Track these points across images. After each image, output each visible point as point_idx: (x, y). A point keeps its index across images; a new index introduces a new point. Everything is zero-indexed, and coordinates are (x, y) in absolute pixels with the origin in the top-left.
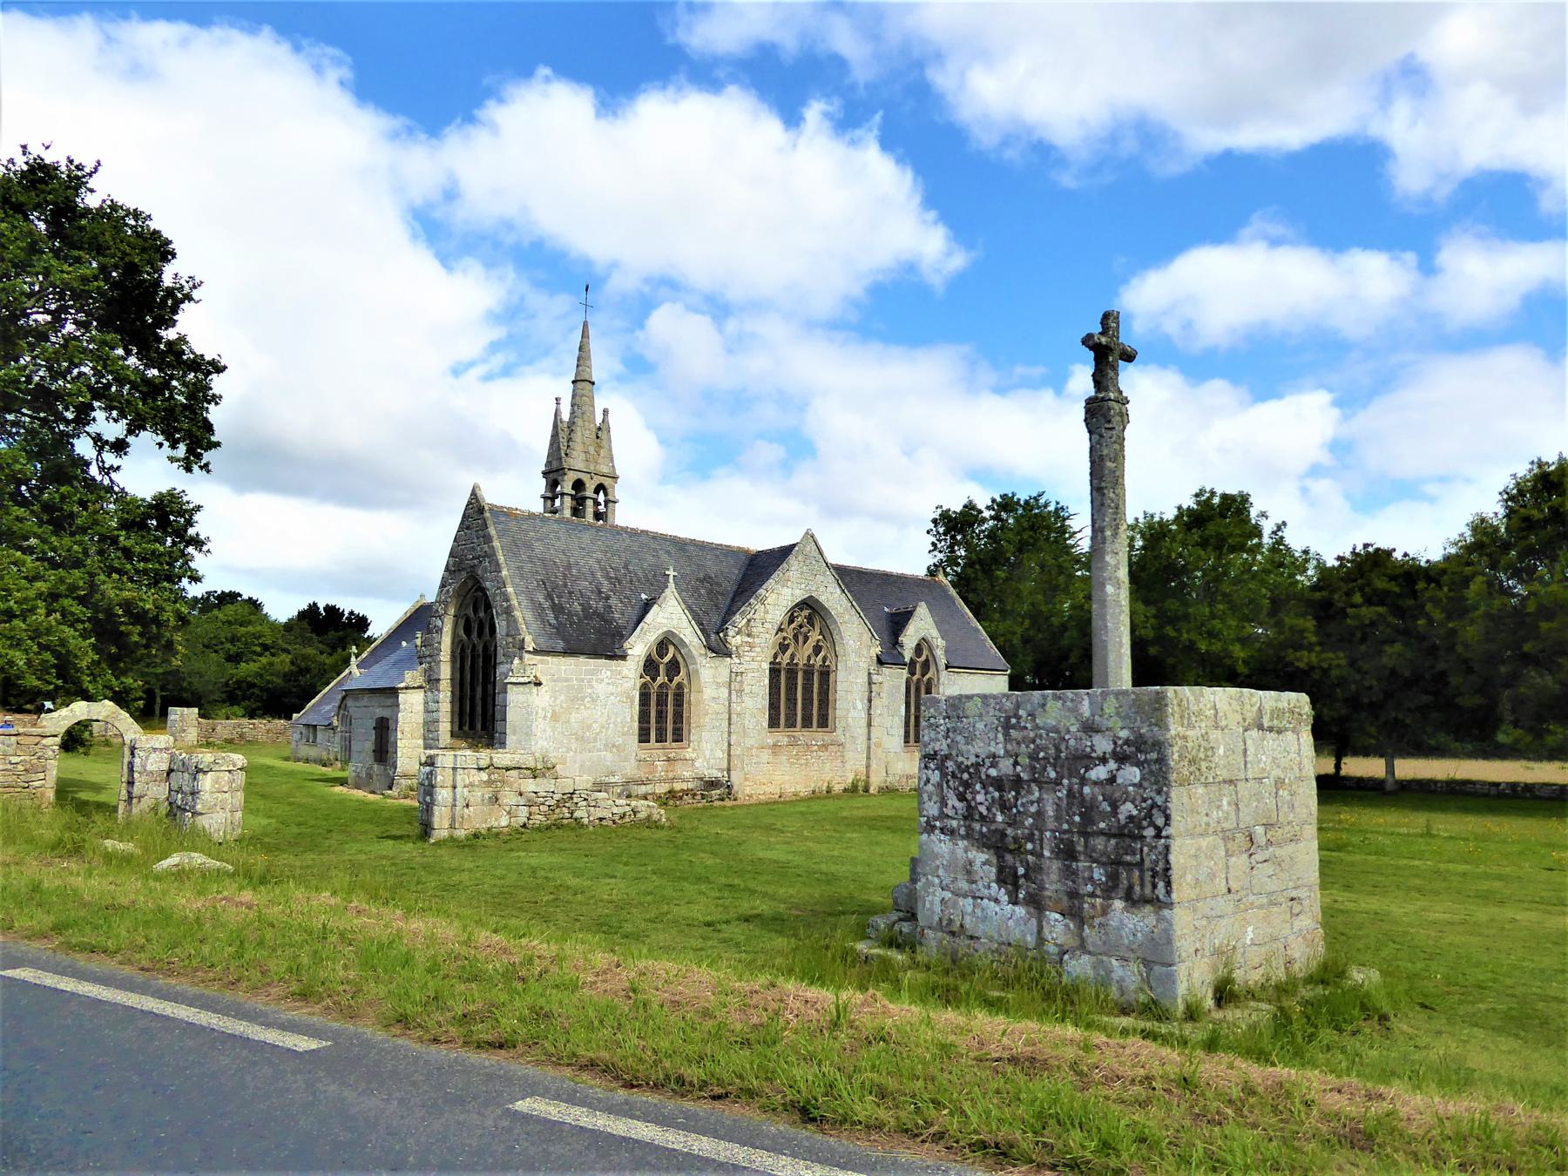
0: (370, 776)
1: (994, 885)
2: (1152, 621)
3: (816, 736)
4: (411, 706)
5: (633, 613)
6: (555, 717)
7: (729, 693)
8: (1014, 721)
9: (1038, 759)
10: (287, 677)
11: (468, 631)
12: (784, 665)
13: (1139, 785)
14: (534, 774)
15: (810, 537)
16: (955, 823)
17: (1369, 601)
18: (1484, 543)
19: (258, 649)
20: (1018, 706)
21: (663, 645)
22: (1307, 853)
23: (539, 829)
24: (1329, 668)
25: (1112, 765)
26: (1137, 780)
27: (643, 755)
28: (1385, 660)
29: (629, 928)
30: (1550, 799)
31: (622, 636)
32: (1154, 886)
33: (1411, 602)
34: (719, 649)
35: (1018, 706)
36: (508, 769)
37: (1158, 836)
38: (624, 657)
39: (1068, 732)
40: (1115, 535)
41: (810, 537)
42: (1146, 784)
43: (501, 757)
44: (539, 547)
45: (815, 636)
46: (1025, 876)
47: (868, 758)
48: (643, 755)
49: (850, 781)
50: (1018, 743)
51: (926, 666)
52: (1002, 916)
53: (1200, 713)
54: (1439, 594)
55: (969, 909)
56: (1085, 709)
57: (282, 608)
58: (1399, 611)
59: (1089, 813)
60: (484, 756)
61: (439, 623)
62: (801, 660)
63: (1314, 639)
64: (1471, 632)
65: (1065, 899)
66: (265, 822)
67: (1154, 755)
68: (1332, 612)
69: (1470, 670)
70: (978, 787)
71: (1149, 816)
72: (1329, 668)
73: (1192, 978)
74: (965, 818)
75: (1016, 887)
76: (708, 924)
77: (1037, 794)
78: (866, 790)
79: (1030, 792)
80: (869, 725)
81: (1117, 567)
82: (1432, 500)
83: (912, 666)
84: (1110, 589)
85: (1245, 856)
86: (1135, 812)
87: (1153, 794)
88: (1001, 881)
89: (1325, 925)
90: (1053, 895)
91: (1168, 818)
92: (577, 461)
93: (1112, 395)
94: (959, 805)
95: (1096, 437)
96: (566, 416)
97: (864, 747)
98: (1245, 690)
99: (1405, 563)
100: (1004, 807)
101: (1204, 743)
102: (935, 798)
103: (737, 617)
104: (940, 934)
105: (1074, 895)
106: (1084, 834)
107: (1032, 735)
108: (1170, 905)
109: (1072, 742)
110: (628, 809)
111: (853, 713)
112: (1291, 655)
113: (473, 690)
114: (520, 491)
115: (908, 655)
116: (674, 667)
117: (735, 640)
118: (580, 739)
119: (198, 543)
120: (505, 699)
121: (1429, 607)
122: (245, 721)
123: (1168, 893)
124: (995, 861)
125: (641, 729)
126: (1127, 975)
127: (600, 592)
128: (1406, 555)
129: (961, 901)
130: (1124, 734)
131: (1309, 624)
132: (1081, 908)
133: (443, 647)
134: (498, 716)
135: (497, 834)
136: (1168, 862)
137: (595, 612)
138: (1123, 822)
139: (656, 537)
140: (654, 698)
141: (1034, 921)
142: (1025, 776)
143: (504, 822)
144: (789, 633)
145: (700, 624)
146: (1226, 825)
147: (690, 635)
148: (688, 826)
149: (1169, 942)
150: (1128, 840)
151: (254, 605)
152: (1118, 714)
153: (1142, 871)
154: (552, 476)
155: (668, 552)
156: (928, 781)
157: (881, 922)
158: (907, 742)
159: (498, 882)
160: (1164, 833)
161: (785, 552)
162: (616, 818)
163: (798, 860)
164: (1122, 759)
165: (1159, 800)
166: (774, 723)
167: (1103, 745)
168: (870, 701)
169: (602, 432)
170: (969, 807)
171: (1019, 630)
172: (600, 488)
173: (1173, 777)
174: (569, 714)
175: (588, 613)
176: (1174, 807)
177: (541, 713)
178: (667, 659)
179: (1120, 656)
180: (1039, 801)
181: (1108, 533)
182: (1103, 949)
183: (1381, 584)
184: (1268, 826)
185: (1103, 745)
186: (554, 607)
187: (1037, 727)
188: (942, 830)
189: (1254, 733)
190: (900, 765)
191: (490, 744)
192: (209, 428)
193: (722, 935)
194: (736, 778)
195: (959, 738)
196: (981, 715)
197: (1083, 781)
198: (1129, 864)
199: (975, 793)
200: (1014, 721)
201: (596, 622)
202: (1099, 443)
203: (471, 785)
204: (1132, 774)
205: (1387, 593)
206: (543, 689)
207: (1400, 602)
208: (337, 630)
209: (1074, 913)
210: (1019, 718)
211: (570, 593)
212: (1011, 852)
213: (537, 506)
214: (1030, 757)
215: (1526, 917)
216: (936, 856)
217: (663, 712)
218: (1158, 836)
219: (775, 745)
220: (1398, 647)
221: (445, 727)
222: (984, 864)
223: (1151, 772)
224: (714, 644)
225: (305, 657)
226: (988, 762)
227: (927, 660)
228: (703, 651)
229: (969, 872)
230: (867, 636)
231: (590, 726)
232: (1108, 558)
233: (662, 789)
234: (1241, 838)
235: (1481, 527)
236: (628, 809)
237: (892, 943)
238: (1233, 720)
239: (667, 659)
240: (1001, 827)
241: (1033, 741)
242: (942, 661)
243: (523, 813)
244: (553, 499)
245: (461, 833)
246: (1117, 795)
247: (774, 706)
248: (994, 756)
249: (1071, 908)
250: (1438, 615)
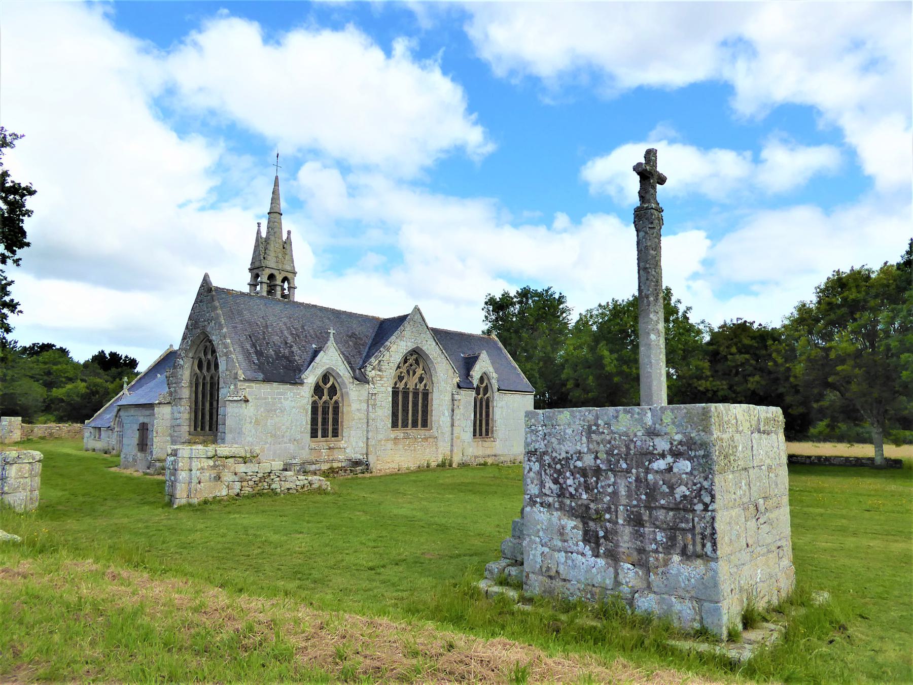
0: (135, 460)
1: (581, 543)
2: (615, 362)
3: (420, 432)
4: (163, 416)
5: (307, 357)
6: (257, 423)
7: (367, 407)
8: (594, 428)
9: (613, 455)
10: (83, 396)
11: (200, 366)
12: (401, 389)
13: (691, 473)
14: (245, 460)
15: (417, 310)
16: (551, 500)
17: (740, 352)
18: (805, 318)
19: (64, 380)
20: (597, 418)
21: (325, 377)
22: (783, 514)
23: (248, 497)
24: (717, 391)
25: (669, 459)
26: (689, 470)
27: (313, 445)
28: (749, 385)
29: (316, 574)
30: (840, 465)
31: (300, 371)
32: (704, 546)
33: (764, 352)
34: (361, 378)
35: (597, 418)
36: (226, 458)
37: (706, 509)
38: (302, 384)
39: (636, 436)
40: (656, 300)
41: (417, 310)
42: (696, 473)
43: (223, 450)
44: (247, 315)
45: (419, 371)
46: (605, 537)
47: (452, 446)
48: (313, 445)
49: (440, 460)
50: (598, 443)
51: (486, 390)
52: (585, 568)
53: (728, 422)
54: (781, 347)
55: (563, 560)
56: (649, 419)
57: (81, 354)
58: (757, 357)
59: (652, 492)
60: (211, 449)
61: (181, 362)
62: (411, 386)
63: (708, 373)
64: (799, 368)
65: (635, 553)
66: (60, 494)
67: (702, 453)
68: (718, 357)
69: (797, 392)
70: (568, 474)
71: (699, 495)
72: (717, 391)
73: (729, 612)
74: (559, 496)
75: (598, 545)
76: (371, 569)
77: (613, 480)
78: (450, 465)
79: (607, 478)
80: (452, 425)
81: (657, 322)
82: (756, 294)
83: (478, 390)
84: (653, 337)
85: (754, 520)
86: (688, 493)
87: (701, 480)
88: (586, 540)
89: (794, 563)
90: (626, 551)
91: (713, 497)
92: (271, 262)
93: (653, 206)
94: (554, 487)
95: (642, 234)
96: (264, 235)
97: (450, 439)
98: (751, 406)
99: (759, 330)
100: (588, 489)
101: (732, 443)
102: (535, 482)
103: (372, 359)
104: (540, 577)
105: (641, 551)
106: (648, 508)
107: (608, 438)
108: (716, 560)
109: (639, 443)
110: (306, 482)
111: (442, 418)
112: (695, 383)
113: (203, 405)
114: (235, 277)
115: (475, 383)
116: (333, 391)
117: (371, 374)
118: (274, 436)
119: (12, 306)
120: (225, 411)
121: (774, 355)
122: (53, 425)
123: (715, 551)
124: (581, 526)
125: (312, 429)
126: (684, 611)
127: (286, 343)
128: (760, 325)
129: (556, 554)
130: (678, 437)
131: (707, 364)
132: (647, 561)
133: (184, 378)
134: (220, 422)
135: (220, 501)
136: (713, 528)
137: (283, 356)
138: (678, 500)
139: (322, 309)
140: (320, 410)
141: (611, 570)
142: (603, 467)
143: (224, 493)
144: (404, 369)
145: (349, 363)
146: (745, 500)
147: (343, 370)
148: (345, 492)
149: (716, 585)
150: (682, 513)
151: (63, 352)
152: (673, 423)
153: (694, 535)
154: (255, 271)
155: (329, 319)
156: (531, 469)
157: (495, 566)
158: (474, 435)
159: (220, 539)
160: (710, 508)
161: (402, 319)
162: (299, 488)
163: (419, 514)
164: (677, 455)
165: (706, 484)
166: (395, 425)
167: (662, 445)
168: (453, 411)
169: (286, 246)
170: (561, 488)
171: (536, 368)
172: (285, 279)
173: (716, 468)
174: (267, 421)
175: (278, 356)
176: (717, 489)
177: (248, 420)
178: (328, 385)
179: (660, 382)
180: (614, 484)
181: (652, 299)
182: (664, 590)
183: (747, 341)
184: (765, 498)
185: (662, 445)
186: (257, 352)
187: (612, 432)
188: (542, 504)
189: (756, 435)
190: (471, 450)
191: (215, 441)
192: (24, 234)
193: (382, 577)
194: (372, 459)
195: (553, 440)
196: (569, 424)
197: (648, 471)
198: (684, 530)
199: (565, 478)
200: (594, 428)
201: (284, 362)
202: (644, 237)
203: (202, 469)
204: (684, 466)
205: (751, 346)
206: (250, 404)
207: (758, 352)
208: (117, 368)
209: (642, 563)
210: (598, 426)
211: (268, 343)
212: (593, 520)
213: (246, 289)
214: (607, 453)
215: (877, 544)
216: (537, 522)
217: (326, 419)
218: (706, 509)
219: (395, 438)
220: (757, 378)
221: (185, 429)
222: (573, 528)
223: (700, 464)
224: (358, 376)
225: (96, 385)
226: (575, 458)
227: (487, 386)
228: (351, 380)
229: (562, 534)
230: (451, 371)
231: (279, 428)
232: (651, 316)
233: (325, 467)
234: (752, 508)
235: (803, 309)
236: (306, 482)
237: (503, 582)
238: (745, 427)
239: (328, 385)
240: (586, 502)
241: (610, 442)
242: (496, 387)
243: (238, 485)
244: (255, 286)
245: (195, 501)
246: (673, 480)
247: (395, 415)
248: (580, 453)
249: (639, 560)
250: (780, 360)
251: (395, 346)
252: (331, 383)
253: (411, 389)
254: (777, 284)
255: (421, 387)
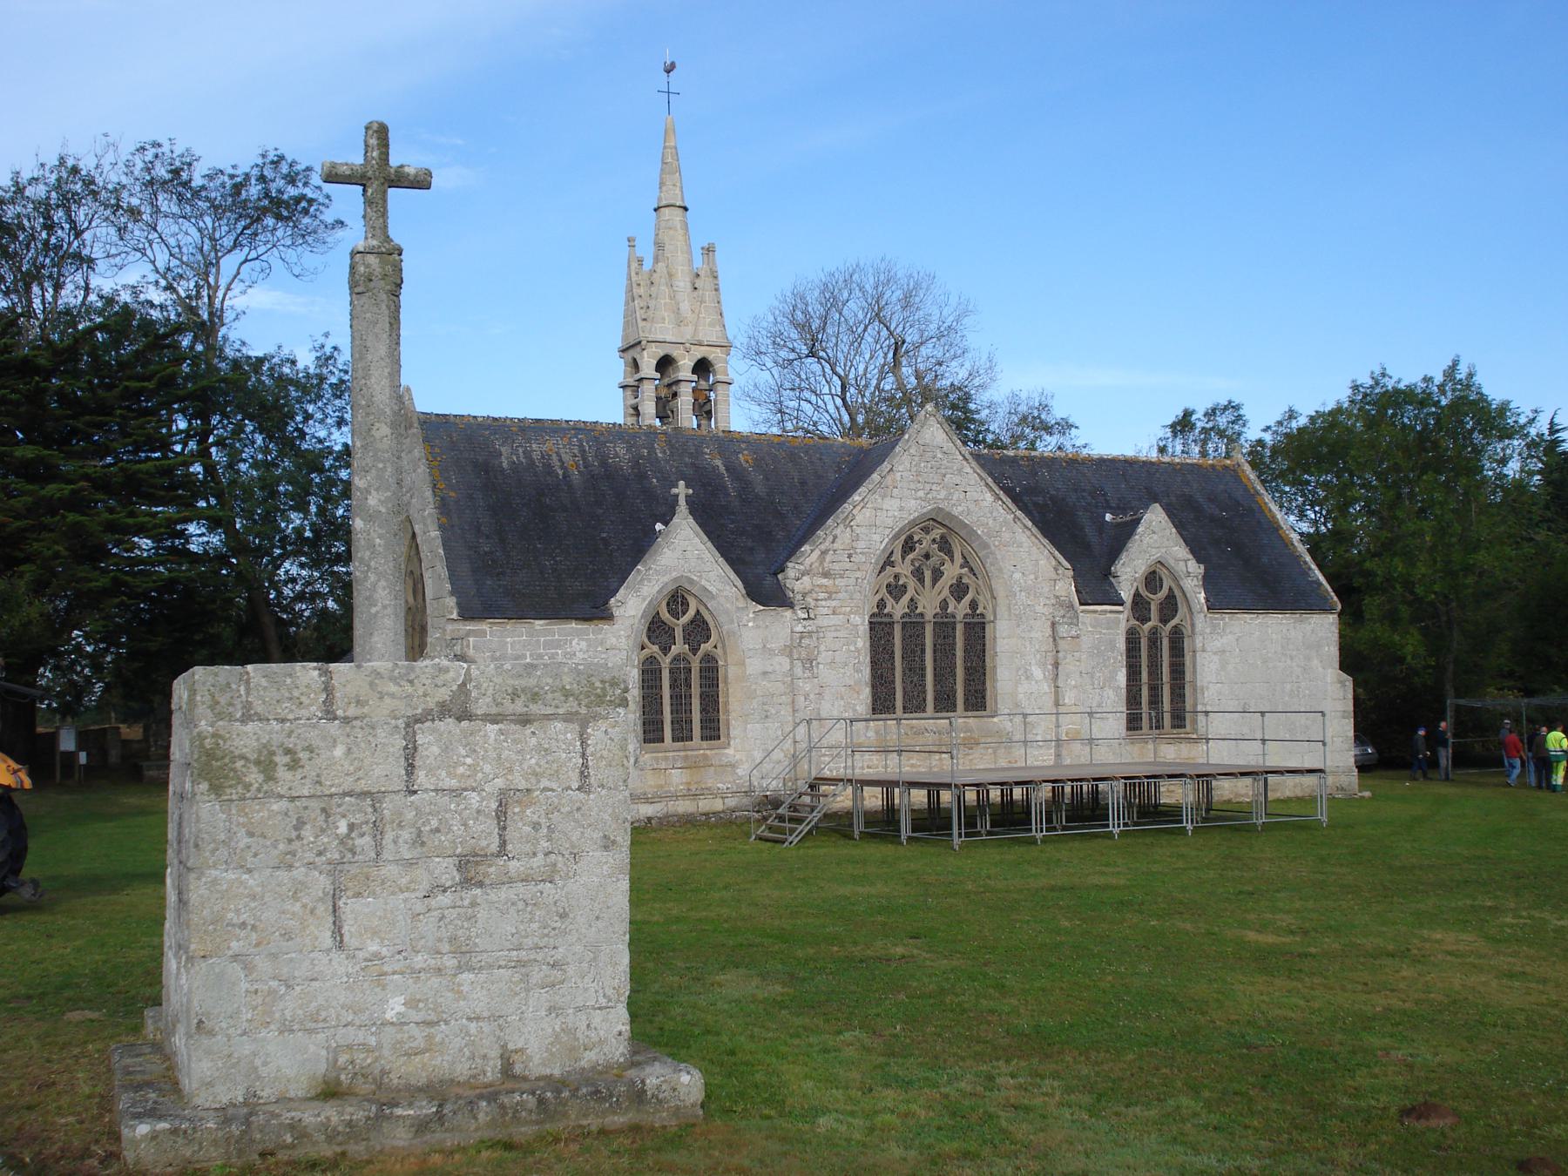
38: (608, 617)
45: (952, 571)
62: (928, 605)
115: (1126, 594)
144: (904, 569)
154: (632, 353)
166: (881, 704)
168: (1056, 665)
227: (1171, 597)
251: (868, 512)
252: (691, 613)
253: (929, 616)
254: (966, 313)
255: (960, 609)
